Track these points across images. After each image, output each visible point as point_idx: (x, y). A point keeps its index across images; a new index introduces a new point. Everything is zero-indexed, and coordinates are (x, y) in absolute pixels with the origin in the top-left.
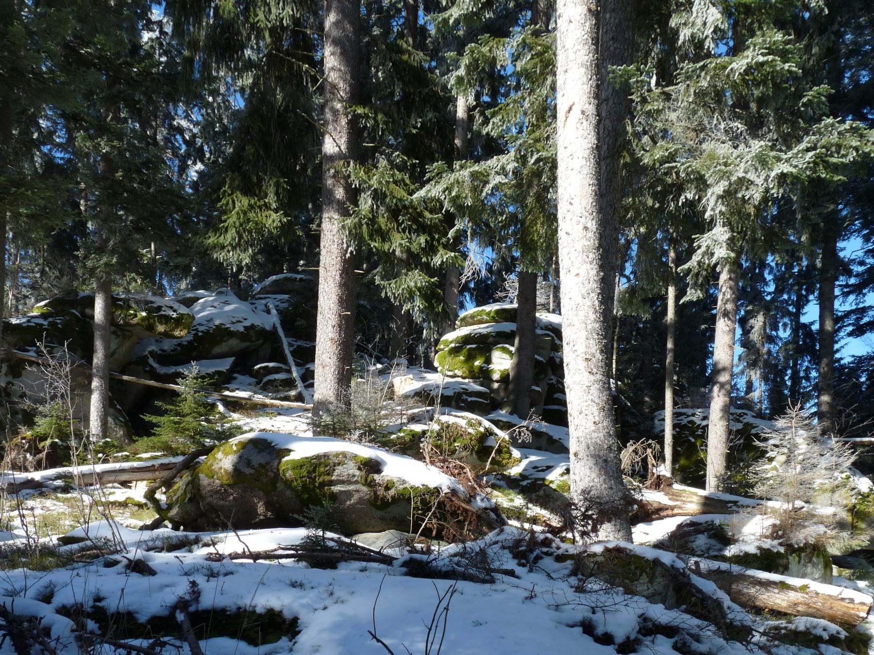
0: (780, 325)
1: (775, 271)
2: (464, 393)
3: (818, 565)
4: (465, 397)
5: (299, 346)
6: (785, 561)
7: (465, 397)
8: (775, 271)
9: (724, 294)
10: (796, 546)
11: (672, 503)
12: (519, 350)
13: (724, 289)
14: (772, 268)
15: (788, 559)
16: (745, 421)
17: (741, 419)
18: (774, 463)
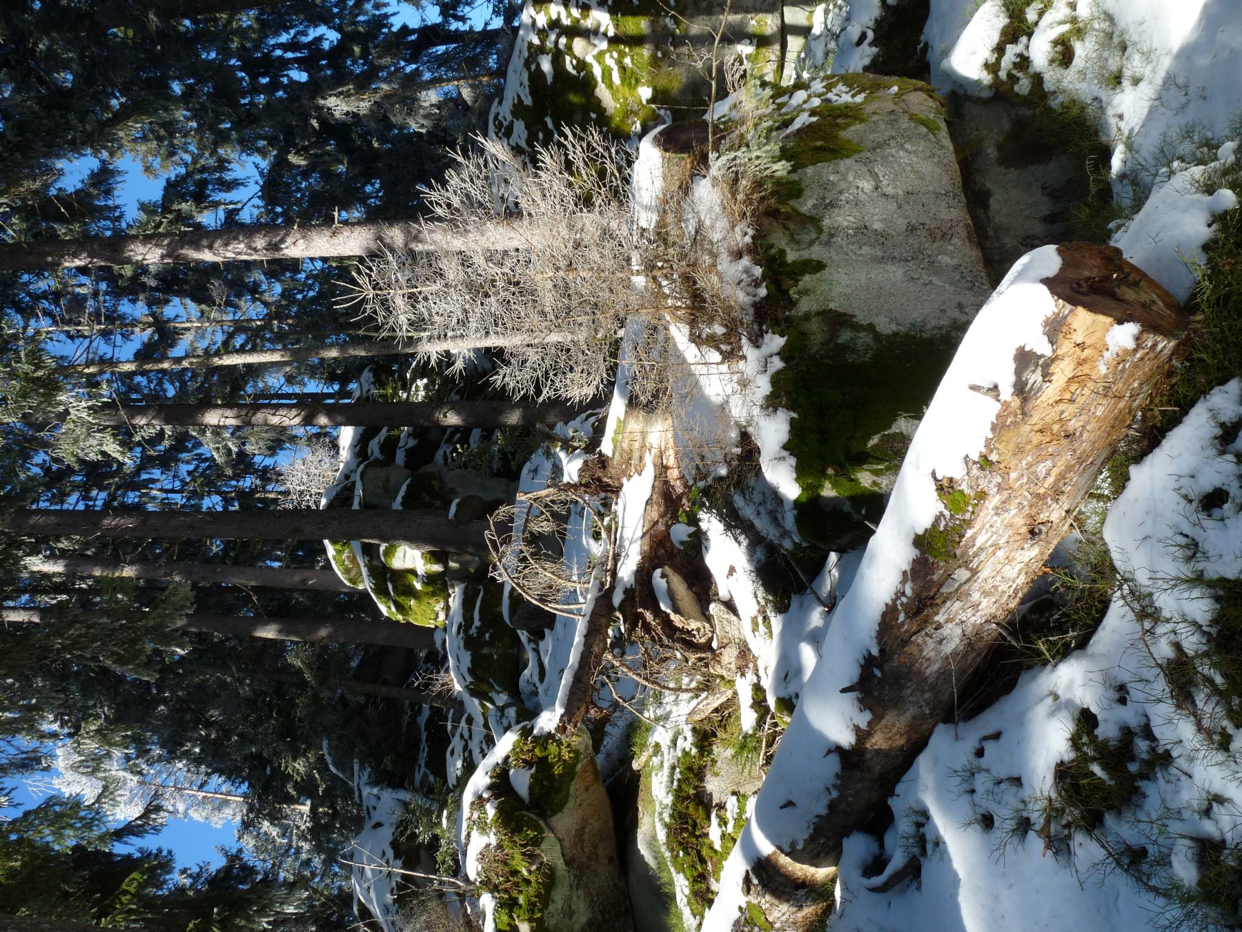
0: (377, 13)
1: (301, 28)
2: (466, 632)
3: (825, 186)
4: (473, 631)
5: (427, 765)
6: (814, 326)
7: (473, 631)
8: (301, 28)
9: (239, 253)
10: (763, 292)
11: (649, 472)
12: (384, 540)
13: (229, 255)
14: (298, 33)
15: (807, 317)
16: (509, 118)
17: (505, 124)
18: (589, 59)
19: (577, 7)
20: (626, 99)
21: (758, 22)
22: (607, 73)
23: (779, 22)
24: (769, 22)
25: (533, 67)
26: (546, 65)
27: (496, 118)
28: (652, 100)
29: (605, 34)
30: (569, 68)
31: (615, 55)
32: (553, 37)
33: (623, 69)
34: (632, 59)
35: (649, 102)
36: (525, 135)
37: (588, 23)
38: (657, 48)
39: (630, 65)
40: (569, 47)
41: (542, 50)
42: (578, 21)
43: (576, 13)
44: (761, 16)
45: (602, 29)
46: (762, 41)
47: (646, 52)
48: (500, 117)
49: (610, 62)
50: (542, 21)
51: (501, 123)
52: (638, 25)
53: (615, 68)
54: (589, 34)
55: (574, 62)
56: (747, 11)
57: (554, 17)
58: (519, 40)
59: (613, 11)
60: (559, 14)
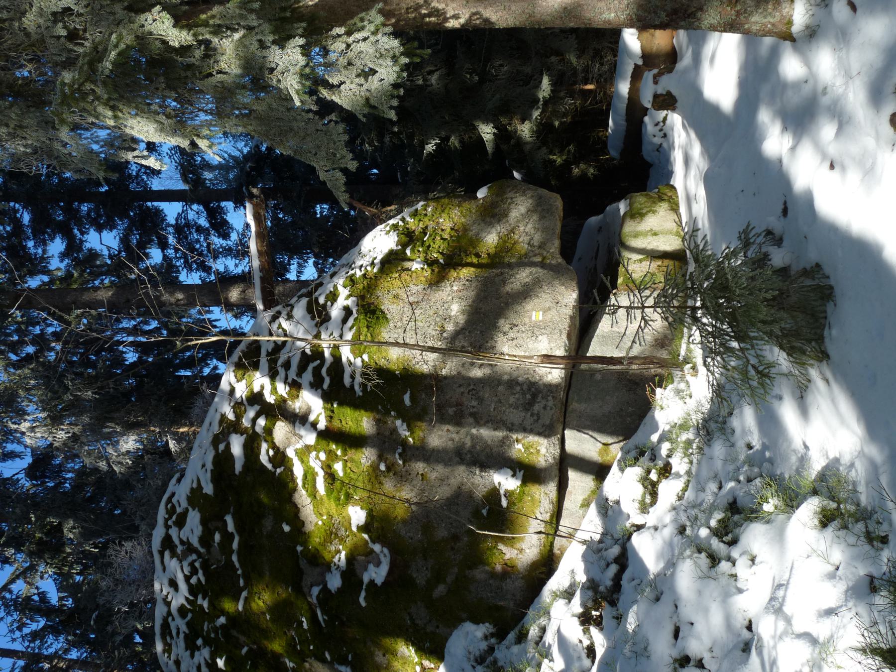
16: (184, 504)
17: (179, 510)
18: (290, 453)
19: (285, 382)
20: (331, 517)
21: (527, 448)
22: (310, 476)
23: (557, 452)
24: (543, 451)
25: (222, 447)
26: (237, 447)
27: (169, 500)
28: (363, 528)
29: (314, 425)
30: (264, 458)
31: (323, 456)
32: (251, 414)
33: (331, 476)
34: (345, 466)
35: (361, 529)
36: (199, 531)
37: (297, 405)
38: (381, 457)
39: (341, 474)
40: (269, 431)
41: (235, 427)
42: (284, 401)
43: (282, 389)
44: (532, 439)
45: (312, 418)
46: (531, 474)
47: (366, 457)
48: (174, 500)
49: (316, 462)
50: (241, 390)
51: (173, 506)
52: (358, 422)
53: (321, 473)
54: (300, 419)
55: (271, 453)
56: (511, 429)
57: (256, 389)
58: (212, 410)
59: (327, 398)
60: (262, 387)
